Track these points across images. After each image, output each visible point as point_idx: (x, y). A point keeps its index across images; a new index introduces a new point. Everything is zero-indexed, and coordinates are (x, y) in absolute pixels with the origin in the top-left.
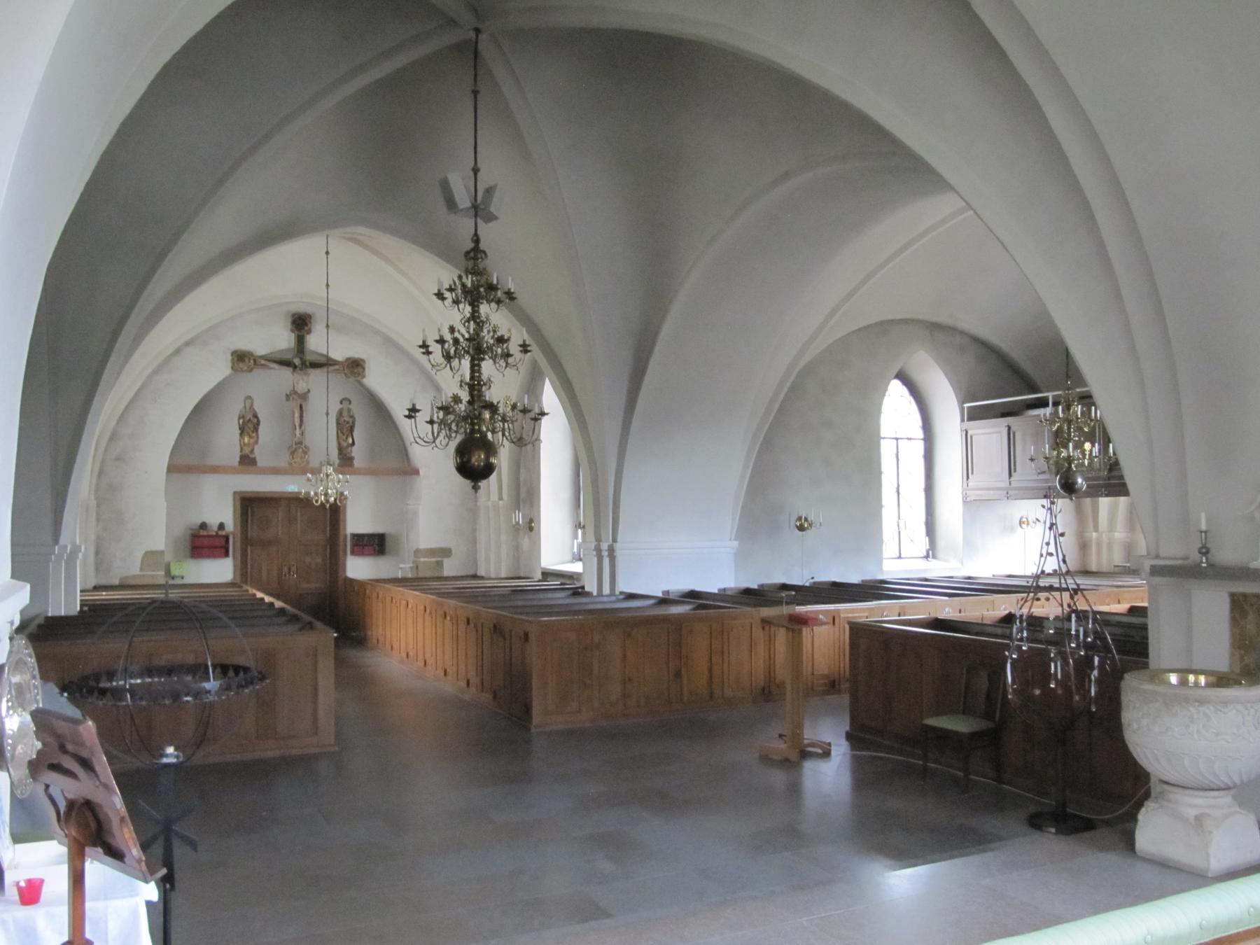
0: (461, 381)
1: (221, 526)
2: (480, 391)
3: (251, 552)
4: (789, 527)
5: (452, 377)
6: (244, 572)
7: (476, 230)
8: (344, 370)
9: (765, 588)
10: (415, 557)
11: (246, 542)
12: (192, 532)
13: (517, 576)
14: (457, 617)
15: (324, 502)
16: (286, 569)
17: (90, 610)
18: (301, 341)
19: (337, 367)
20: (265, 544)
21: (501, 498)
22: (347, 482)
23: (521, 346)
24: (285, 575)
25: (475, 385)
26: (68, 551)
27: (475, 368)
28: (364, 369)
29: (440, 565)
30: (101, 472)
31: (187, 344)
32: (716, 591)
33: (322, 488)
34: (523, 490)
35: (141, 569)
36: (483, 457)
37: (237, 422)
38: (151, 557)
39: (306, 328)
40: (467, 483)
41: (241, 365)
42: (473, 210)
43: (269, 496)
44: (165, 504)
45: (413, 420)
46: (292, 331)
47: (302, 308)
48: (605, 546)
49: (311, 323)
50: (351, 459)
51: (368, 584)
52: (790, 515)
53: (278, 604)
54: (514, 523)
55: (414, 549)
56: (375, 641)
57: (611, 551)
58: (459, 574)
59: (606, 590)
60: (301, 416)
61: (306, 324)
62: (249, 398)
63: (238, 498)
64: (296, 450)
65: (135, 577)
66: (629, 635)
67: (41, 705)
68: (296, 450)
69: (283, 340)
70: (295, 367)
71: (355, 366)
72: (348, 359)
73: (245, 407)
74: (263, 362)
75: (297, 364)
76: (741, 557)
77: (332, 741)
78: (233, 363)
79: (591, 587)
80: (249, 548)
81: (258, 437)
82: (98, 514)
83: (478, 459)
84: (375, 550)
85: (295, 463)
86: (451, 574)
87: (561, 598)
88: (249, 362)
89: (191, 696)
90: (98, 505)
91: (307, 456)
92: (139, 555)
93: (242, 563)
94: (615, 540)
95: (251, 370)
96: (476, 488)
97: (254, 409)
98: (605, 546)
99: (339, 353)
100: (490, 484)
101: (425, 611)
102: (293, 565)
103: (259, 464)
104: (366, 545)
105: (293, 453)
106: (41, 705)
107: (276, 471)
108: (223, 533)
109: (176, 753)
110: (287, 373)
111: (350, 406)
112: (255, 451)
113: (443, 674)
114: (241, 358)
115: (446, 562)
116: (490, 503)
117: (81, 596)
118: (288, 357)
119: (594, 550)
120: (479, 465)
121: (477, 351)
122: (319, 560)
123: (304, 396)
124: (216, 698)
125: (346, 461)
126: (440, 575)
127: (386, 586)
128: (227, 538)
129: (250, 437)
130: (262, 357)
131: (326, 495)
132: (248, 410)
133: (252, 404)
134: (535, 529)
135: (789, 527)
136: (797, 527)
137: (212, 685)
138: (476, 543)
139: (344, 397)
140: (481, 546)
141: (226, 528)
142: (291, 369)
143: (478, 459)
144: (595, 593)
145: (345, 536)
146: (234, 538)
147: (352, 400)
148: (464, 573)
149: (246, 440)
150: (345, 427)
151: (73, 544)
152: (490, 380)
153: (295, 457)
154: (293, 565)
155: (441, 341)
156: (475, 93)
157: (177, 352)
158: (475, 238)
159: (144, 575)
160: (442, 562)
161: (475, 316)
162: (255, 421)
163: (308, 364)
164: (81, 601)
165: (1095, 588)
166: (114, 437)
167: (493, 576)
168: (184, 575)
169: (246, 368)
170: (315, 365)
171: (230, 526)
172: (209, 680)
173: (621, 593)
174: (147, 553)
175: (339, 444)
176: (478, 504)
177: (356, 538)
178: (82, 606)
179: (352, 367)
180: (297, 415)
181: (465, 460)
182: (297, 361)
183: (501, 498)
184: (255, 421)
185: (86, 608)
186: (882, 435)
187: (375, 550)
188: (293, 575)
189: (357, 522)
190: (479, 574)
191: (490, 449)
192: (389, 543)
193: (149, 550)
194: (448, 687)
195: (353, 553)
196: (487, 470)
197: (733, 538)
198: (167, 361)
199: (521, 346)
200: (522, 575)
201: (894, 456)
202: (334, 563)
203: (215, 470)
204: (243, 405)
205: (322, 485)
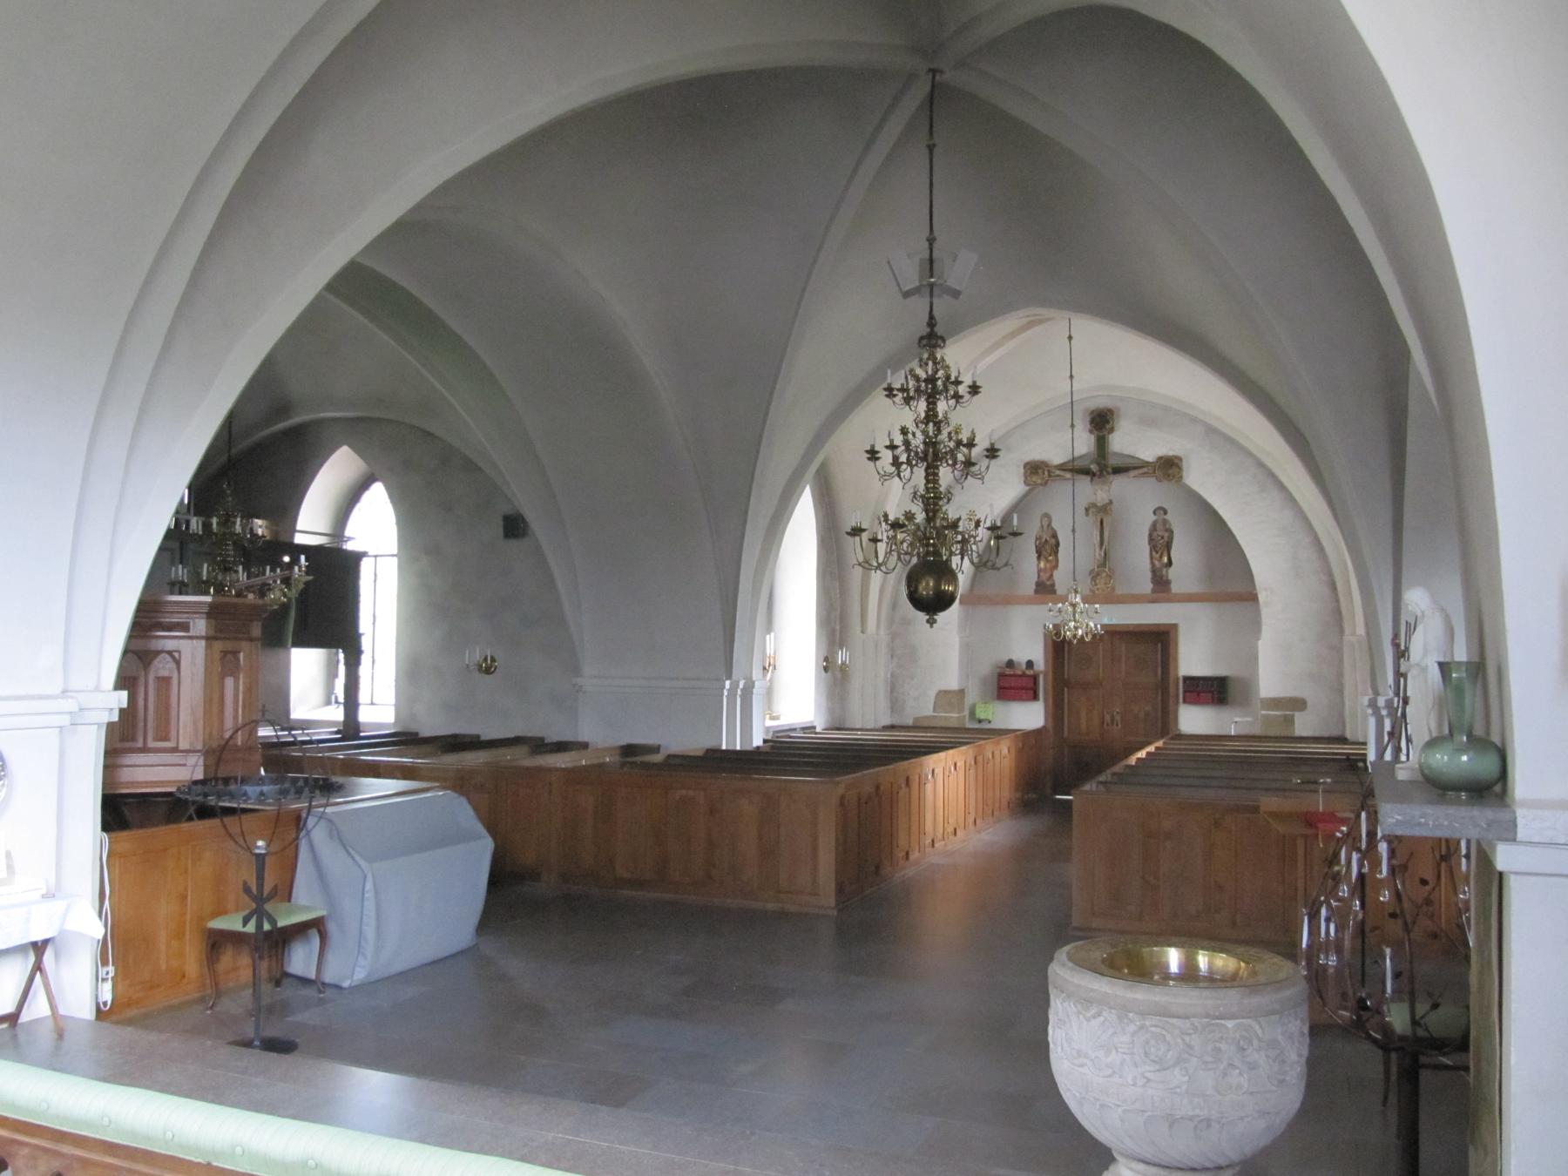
0: (915, 493)
2: (936, 504)
3: (1068, 694)
6: (1056, 712)
8: (1154, 473)
12: (998, 670)
18: (1102, 444)
19: (1145, 470)
22: (1096, 612)
23: (867, 452)
25: (932, 500)
27: (932, 476)
28: (1180, 468)
29: (1289, 721)
35: (934, 710)
36: (931, 584)
38: (948, 698)
39: (1108, 426)
45: (857, 538)
46: (1091, 432)
47: (1102, 403)
49: (1113, 419)
50: (1168, 582)
53: (1132, 760)
61: (1108, 422)
64: (1098, 574)
65: (927, 717)
67: (1346, 895)
69: (1084, 443)
70: (1094, 475)
71: (1169, 467)
72: (1160, 458)
73: (1042, 526)
74: (1058, 472)
75: (1095, 471)
78: (1026, 477)
81: (1057, 561)
85: (1098, 589)
86: (1304, 734)
88: (1044, 473)
91: (1112, 581)
92: (932, 694)
95: (1045, 484)
97: (1052, 529)
99: (1148, 453)
105: (1094, 579)
106: (1346, 895)
108: (1031, 672)
110: (1084, 483)
111: (1166, 517)
114: (1036, 471)
115: (1299, 717)
120: (928, 594)
121: (931, 456)
122: (1148, 708)
125: (1161, 583)
126: (1289, 735)
128: (1035, 678)
129: (1047, 561)
133: (1049, 525)
134: (822, 659)
139: (1157, 506)
141: (1035, 667)
142: (1089, 478)
145: (1178, 679)
147: (1166, 507)
150: (1161, 543)
152: (950, 492)
153: (1098, 581)
155: (892, 447)
156: (931, 148)
159: (936, 717)
160: (1293, 716)
161: (931, 416)
162: (1053, 541)
163: (1110, 470)
165: (972, 740)
169: (1039, 481)
170: (1118, 471)
174: (940, 692)
175: (1153, 564)
181: (912, 589)
184: (1053, 541)
186: (396, 559)
189: (1193, 660)
195: (1185, 701)
199: (867, 452)
201: (378, 577)
204: (1040, 524)
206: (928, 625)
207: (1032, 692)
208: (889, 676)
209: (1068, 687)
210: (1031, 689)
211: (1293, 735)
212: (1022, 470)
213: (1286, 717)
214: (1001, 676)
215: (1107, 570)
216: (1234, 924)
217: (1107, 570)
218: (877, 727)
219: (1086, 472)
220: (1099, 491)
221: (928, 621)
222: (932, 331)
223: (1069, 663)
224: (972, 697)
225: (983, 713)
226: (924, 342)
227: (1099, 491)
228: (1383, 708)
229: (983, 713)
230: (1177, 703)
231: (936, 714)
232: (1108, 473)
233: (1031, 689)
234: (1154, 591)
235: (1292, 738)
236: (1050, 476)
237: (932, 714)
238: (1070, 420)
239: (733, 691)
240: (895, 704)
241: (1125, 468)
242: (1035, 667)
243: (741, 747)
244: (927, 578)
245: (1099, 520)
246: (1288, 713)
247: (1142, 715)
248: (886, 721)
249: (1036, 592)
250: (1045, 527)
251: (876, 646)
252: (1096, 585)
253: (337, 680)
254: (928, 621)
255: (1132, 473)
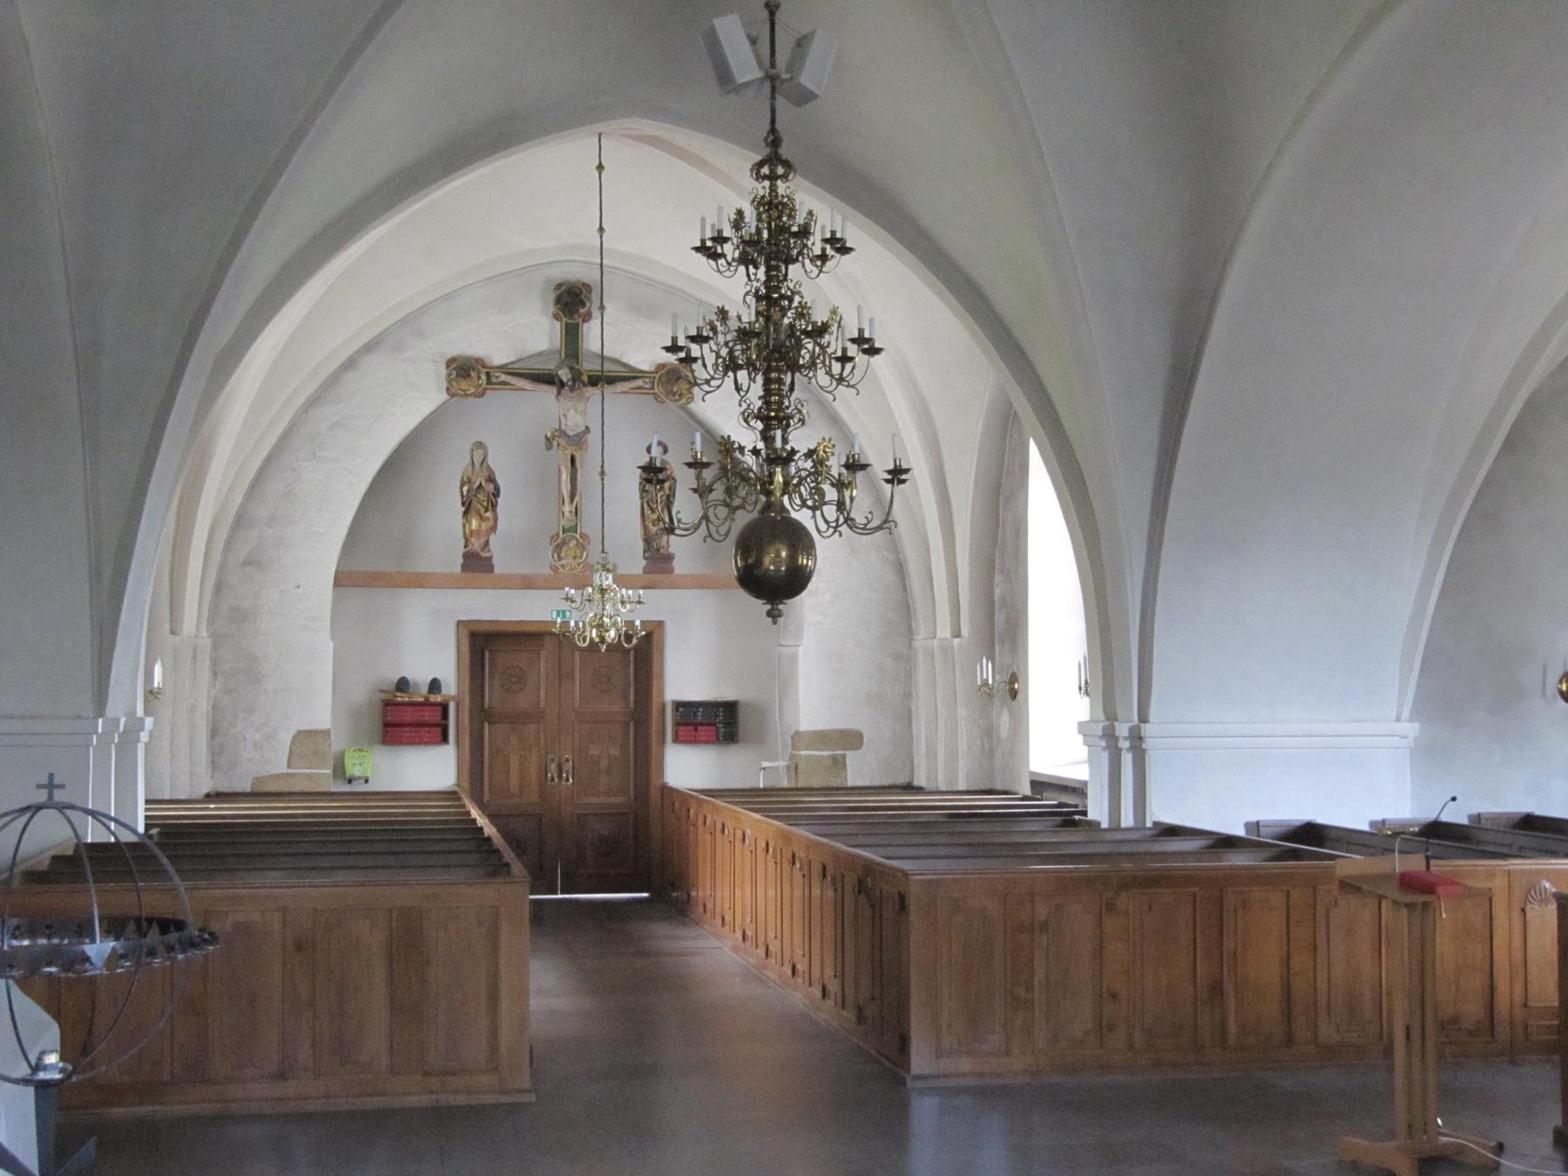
1: (435, 686)
4: (1544, 694)
5: (737, 404)
6: (475, 768)
7: (773, 121)
8: (653, 388)
9: (1484, 824)
10: (793, 749)
11: (482, 714)
13: (988, 787)
14: (810, 862)
15: (597, 640)
16: (553, 767)
17: (160, 834)
18: (572, 335)
19: (639, 383)
20: (518, 719)
21: (957, 634)
24: (553, 780)
26: (121, 729)
29: (839, 764)
30: (219, 588)
31: (370, 347)
32: (1364, 827)
33: (591, 615)
34: (999, 618)
35: (289, 766)
37: (458, 490)
38: (308, 741)
39: (582, 311)
40: (761, 607)
41: (464, 384)
42: (769, 82)
43: (528, 629)
44: (331, 644)
46: (556, 317)
48: (1122, 730)
50: (669, 558)
51: (691, 796)
52: (1545, 670)
53: (489, 830)
54: (979, 683)
55: (791, 733)
56: (701, 909)
57: (1137, 738)
58: (876, 783)
59: (1127, 820)
60: (573, 480)
61: (583, 304)
62: (480, 445)
63: (465, 632)
64: (564, 543)
66: (1110, 907)
68: (564, 543)
70: (562, 385)
74: (503, 378)
75: (565, 380)
76: (1428, 755)
77: (526, 1085)
78: (449, 382)
79: (1097, 811)
80: (486, 725)
81: (496, 520)
82: (215, 663)
83: (775, 559)
84: (717, 733)
85: (563, 566)
87: (1041, 833)
88: (479, 378)
89: (57, 966)
90: (215, 647)
92: (286, 738)
93: (472, 754)
94: (1143, 719)
96: (774, 615)
97: (488, 466)
98: (1122, 730)
100: (806, 604)
101: (767, 851)
102: (567, 760)
103: (497, 570)
104: (702, 724)
105: (558, 548)
107: (528, 583)
108: (439, 699)
109: (61, 1065)
112: (491, 543)
113: (790, 972)
114: (464, 370)
116: (936, 642)
117: (147, 810)
118: (550, 365)
119: (1102, 737)
120: (777, 570)
122: (615, 751)
123: (579, 440)
124: (105, 972)
125: (658, 561)
127: (718, 802)
128: (444, 707)
129: (482, 518)
130: (504, 368)
131: (600, 626)
132: (477, 465)
135: (1544, 694)
136: (1562, 693)
137: (99, 949)
138: (910, 720)
140: (920, 729)
142: (553, 390)
143: (775, 559)
144: (1105, 825)
146: (458, 705)
148: (886, 782)
149: (474, 524)
151: (131, 714)
153: (562, 555)
154: (567, 760)
157: (350, 364)
158: (771, 137)
159: (293, 775)
160: (844, 757)
162: (490, 488)
163: (585, 378)
164: (147, 817)
166: (241, 521)
167: (943, 788)
168: (369, 775)
170: (594, 381)
171: (450, 687)
172: (93, 941)
173: (1156, 824)
174: (299, 733)
175: (645, 528)
176: (915, 644)
177: (681, 709)
178: (148, 827)
179: (668, 381)
180: (565, 476)
181: (750, 561)
182: (564, 374)
183: (957, 634)
184: (490, 488)
185: (154, 831)
187: (717, 733)
188: (567, 780)
190: (916, 783)
191: (798, 539)
192: (745, 722)
193: (305, 728)
194: (800, 997)
195: (677, 739)
196: (795, 581)
197: (1406, 714)
198: (333, 380)
200: (999, 787)
202: (644, 761)
203: (418, 581)
204: (468, 460)
205: (591, 609)
206: (770, 620)
207: (439, 729)
208: (210, 708)
209: (490, 723)
210: (438, 725)
211: (844, 786)
212: (443, 371)
213: (834, 758)
214: (388, 704)
215: (578, 536)
216: (1131, 1047)
217: (578, 536)
218: (195, 796)
219: (547, 379)
220: (572, 411)
221: (769, 614)
222: (776, 153)
223: (490, 682)
224: (337, 744)
225: (358, 767)
226: (765, 170)
227: (572, 411)
228: (1126, 738)
229: (358, 767)
230: (663, 742)
231: (291, 771)
232: (585, 385)
233: (438, 725)
234: (647, 571)
235: (842, 789)
236: (489, 382)
237: (285, 770)
238: (599, 301)
239: (106, 739)
240: (216, 761)
241: (607, 377)
242: (444, 691)
243: (92, 839)
244: (778, 546)
245: (569, 457)
246: (838, 752)
247: (604, 764)
248: (206, 787)
249: (465, 567)
250: (477, 465)
251: (195, 657)
252: (560, 558)
253: (151, 728)
254: (769, 614)
255: (621, 387)
